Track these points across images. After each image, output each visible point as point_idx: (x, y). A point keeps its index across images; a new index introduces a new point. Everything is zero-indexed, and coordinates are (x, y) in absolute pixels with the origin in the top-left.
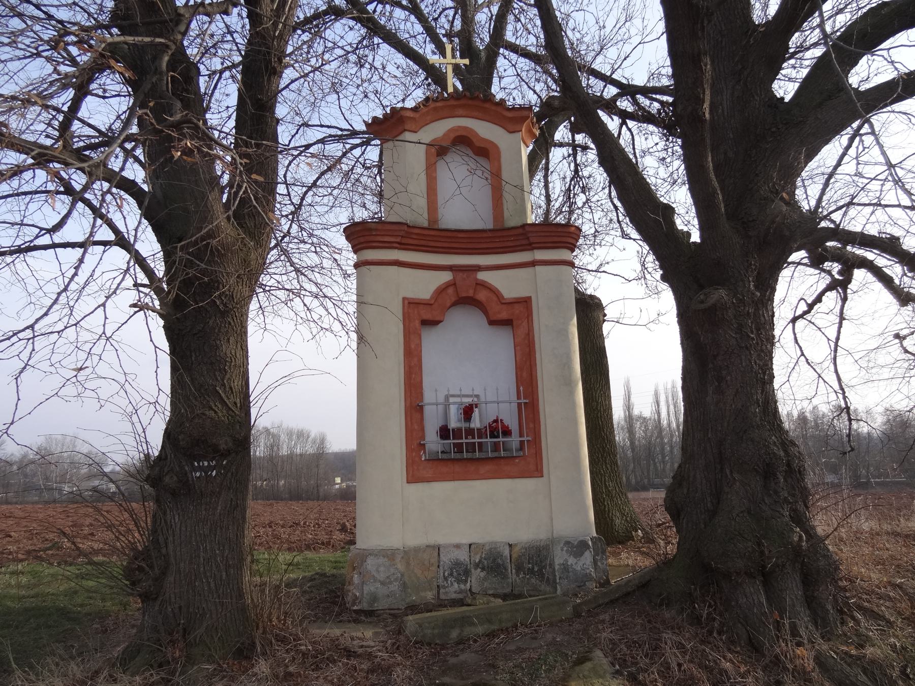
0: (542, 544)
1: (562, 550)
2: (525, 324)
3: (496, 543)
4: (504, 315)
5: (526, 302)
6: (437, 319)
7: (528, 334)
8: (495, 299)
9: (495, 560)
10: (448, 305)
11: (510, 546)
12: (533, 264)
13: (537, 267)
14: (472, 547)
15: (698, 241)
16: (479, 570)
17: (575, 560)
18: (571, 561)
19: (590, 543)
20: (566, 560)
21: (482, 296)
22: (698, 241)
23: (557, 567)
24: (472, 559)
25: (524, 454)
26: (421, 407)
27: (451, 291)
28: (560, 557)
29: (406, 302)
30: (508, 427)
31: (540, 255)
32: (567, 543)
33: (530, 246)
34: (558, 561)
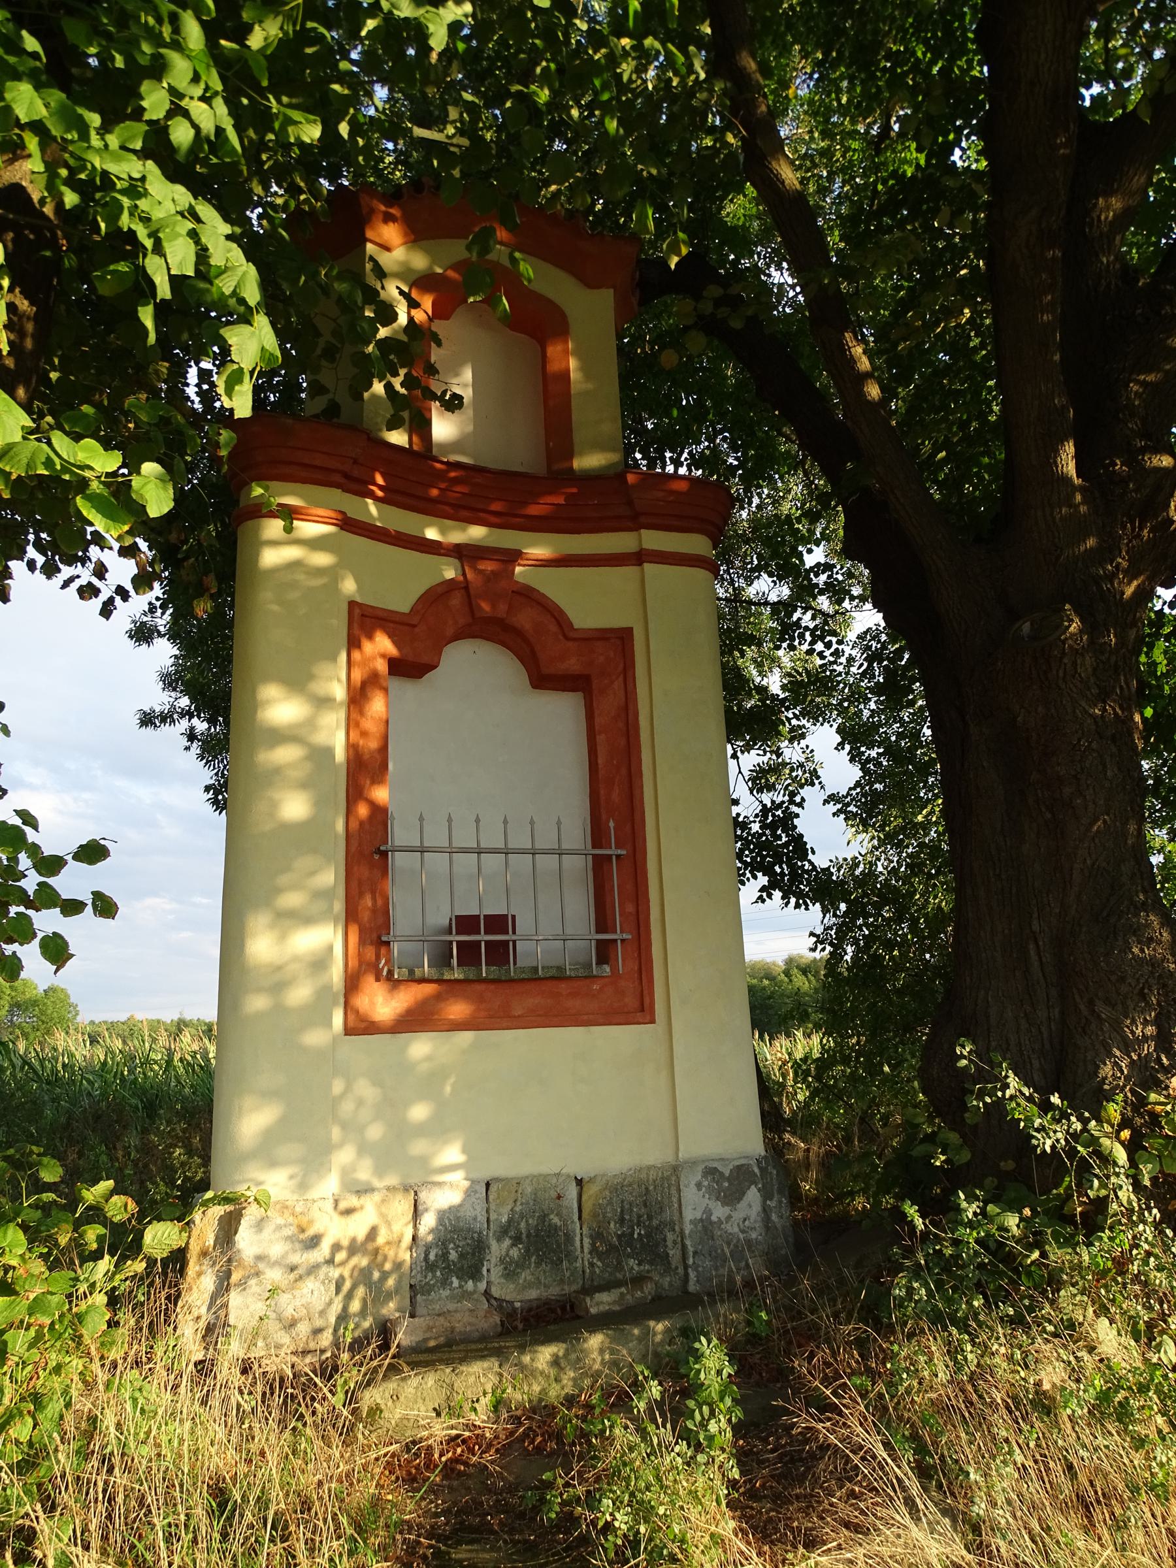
0: (653, 1175)
1: (699, 1186)
2: (618, 684)
3: (546, 1177)
4: (572, 665)
5: (622, 639)
6: (426, 659)
7: (626, 708)
8: (553, 628)
9: (544, 1217)
10: (450, 631)
11: (579, 1182)
12: (639, 558)
13: (647, 566)
14: (493, 1188)
15: (168, 296)
16: (507, 1242)
17: (727, 1209)
18: (719, 1212)
19: (756, 1170)
20: (708, 1212)
21: (525, 619)
22: (168, 296)
23: (688, 1228)
24: (493, 1217)
25: (614, 969)
26: (384, 854)
27: (456, 600)
28: (695, 1203)
29: (357, 611)
30: (454, 1253)
31: (653, 540)
32: (711, 1172)
33: (634, 521)
34: (690, 1214)
